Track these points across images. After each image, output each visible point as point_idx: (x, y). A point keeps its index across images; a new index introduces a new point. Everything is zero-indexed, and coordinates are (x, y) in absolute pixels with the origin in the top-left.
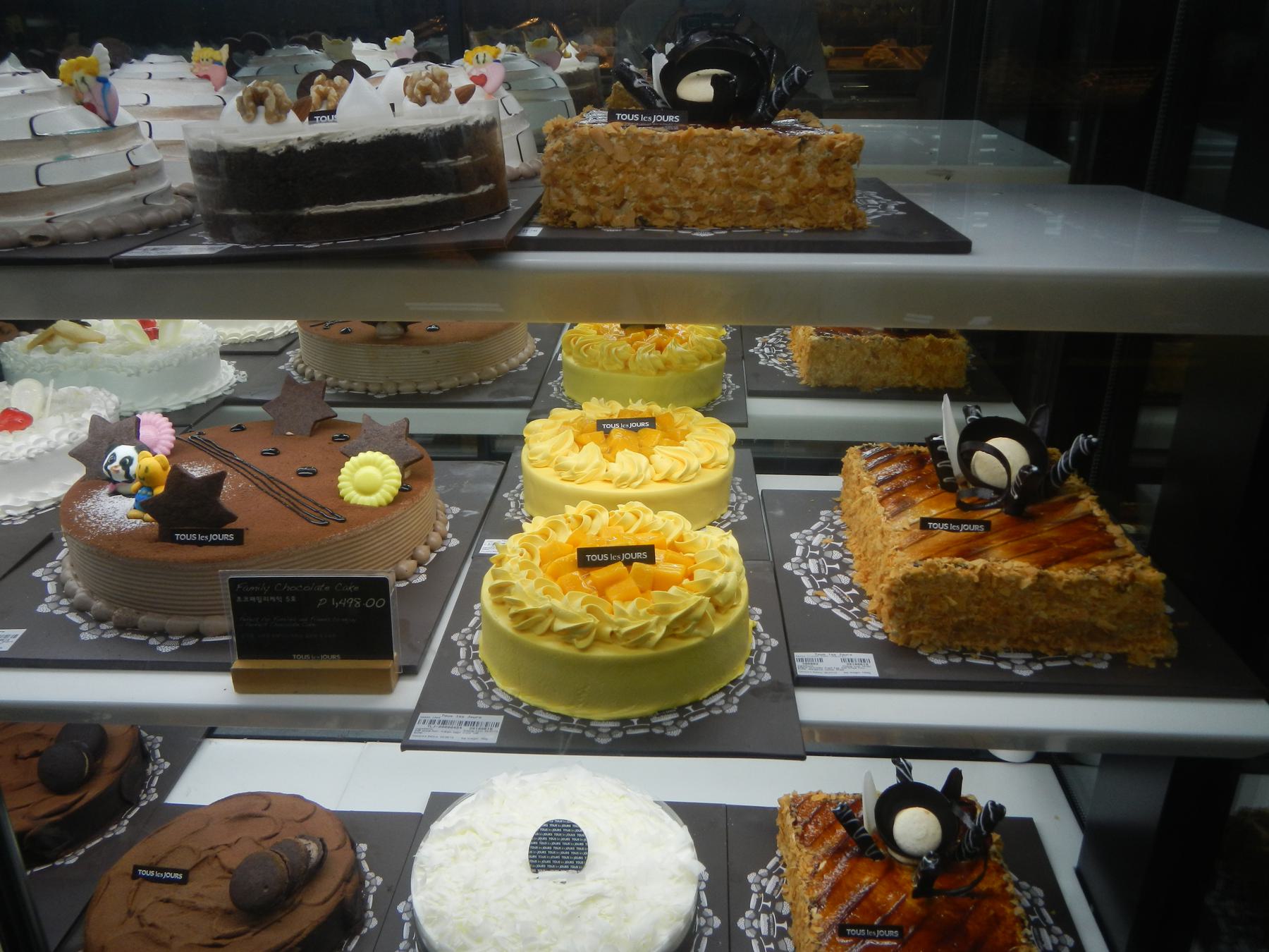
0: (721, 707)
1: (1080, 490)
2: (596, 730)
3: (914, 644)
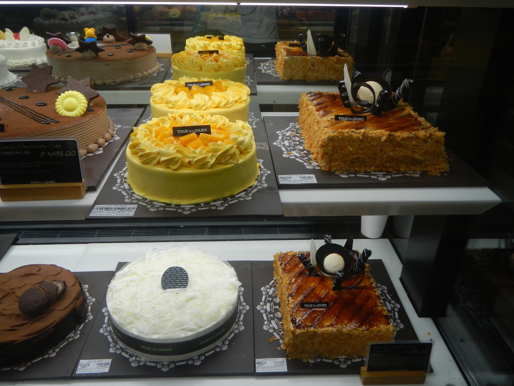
0: (244, 198)
1: (405, 106)
2: (183, 209)
3: (333, 170)
